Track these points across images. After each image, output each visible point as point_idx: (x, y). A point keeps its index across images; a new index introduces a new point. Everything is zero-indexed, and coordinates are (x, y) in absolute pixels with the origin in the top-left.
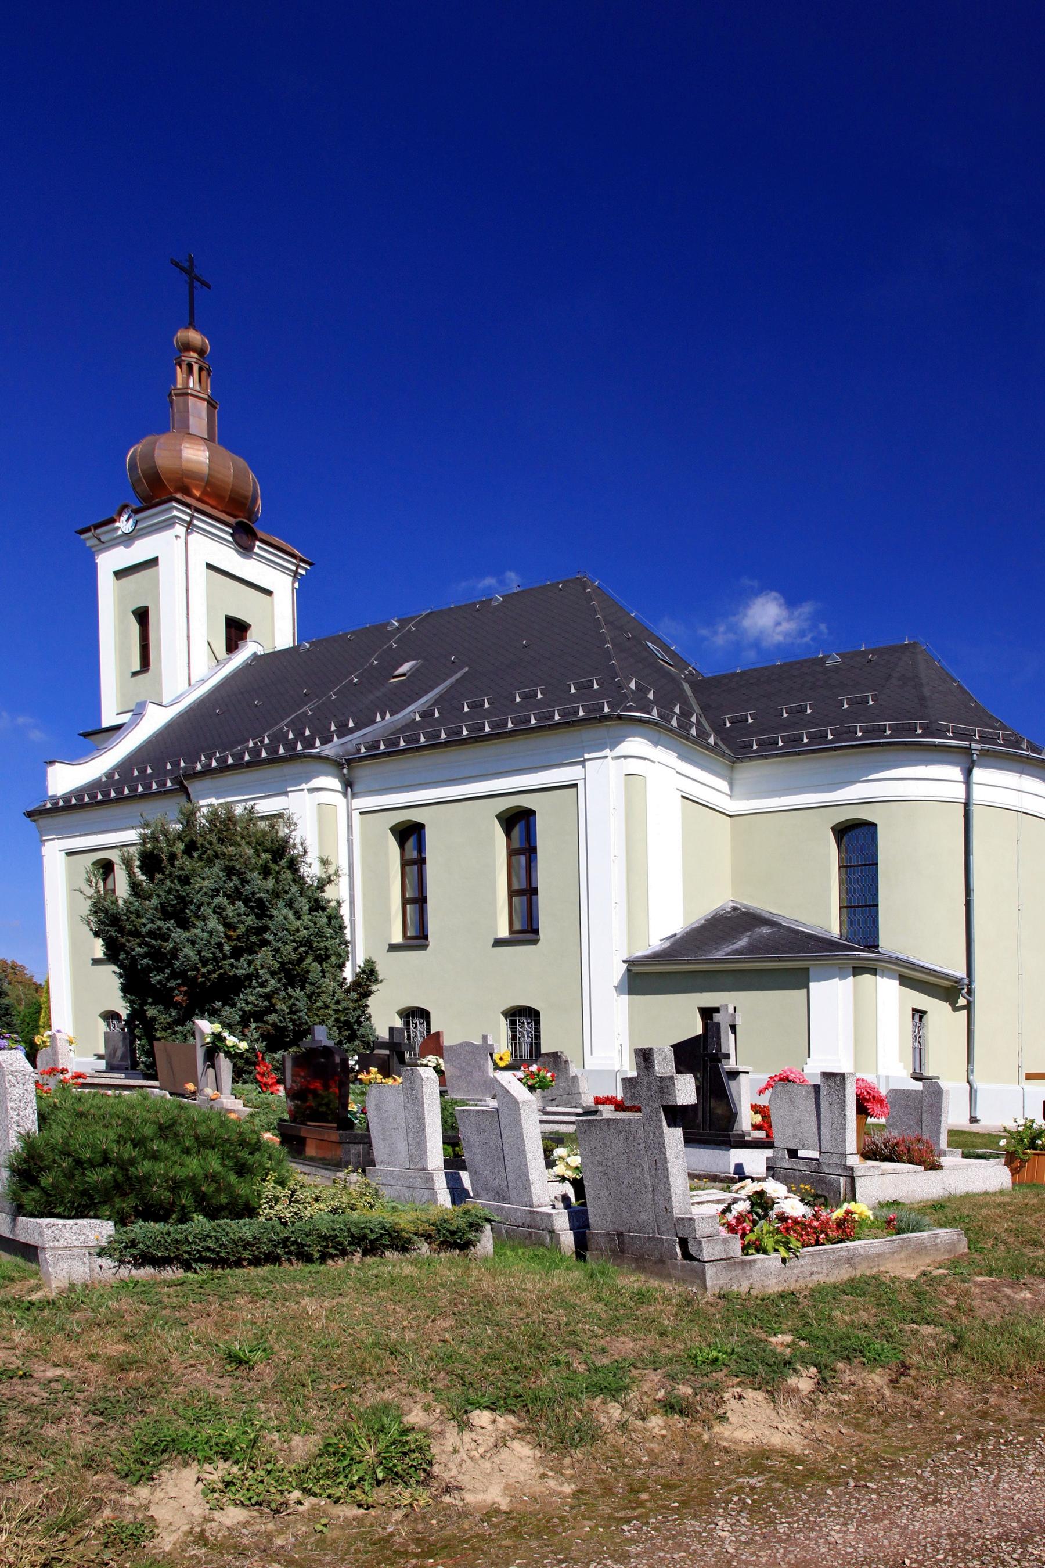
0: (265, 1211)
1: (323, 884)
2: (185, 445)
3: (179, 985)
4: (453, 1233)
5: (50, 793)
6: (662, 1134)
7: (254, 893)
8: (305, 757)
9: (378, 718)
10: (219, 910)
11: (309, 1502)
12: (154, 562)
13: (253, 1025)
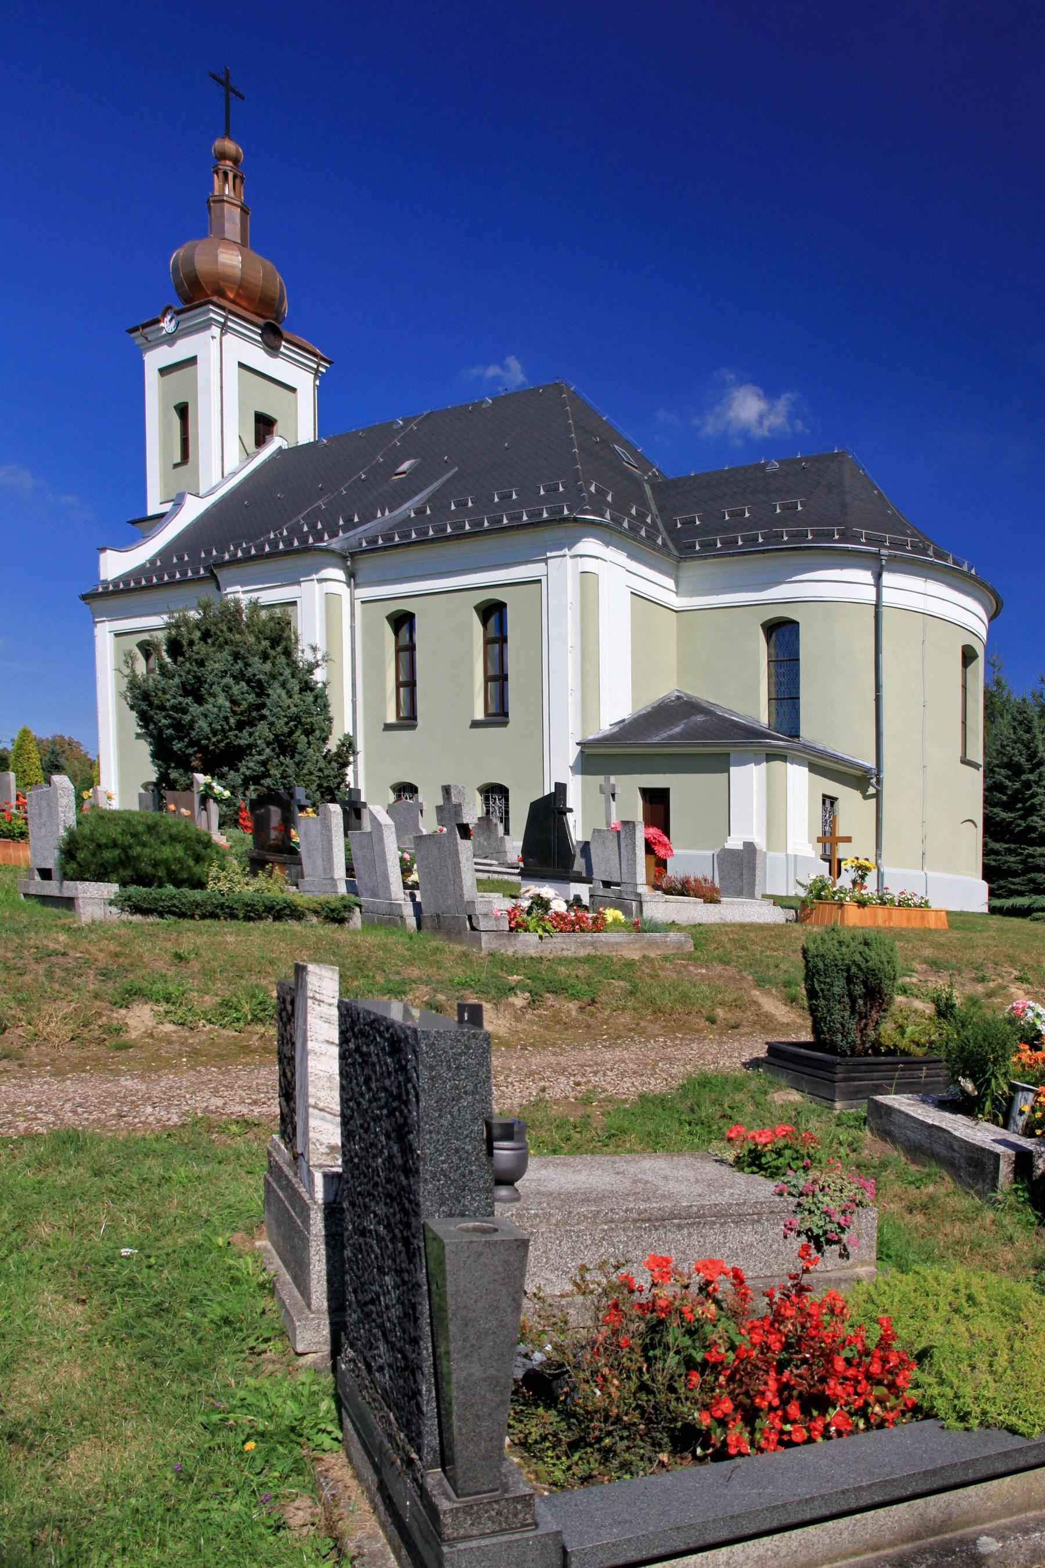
0: (211, 885)
1: (312, 667)
2: (221, 250)
3: (195, 752)
4: (333, 911)
5: (102, 578)
6: (456, 844)
7: (254, 675)
8: (315, 550)
9: (379, 515)
10: (226, 689)
11: (208, 1027)
12: (193, 361)
13: (252, 788)
